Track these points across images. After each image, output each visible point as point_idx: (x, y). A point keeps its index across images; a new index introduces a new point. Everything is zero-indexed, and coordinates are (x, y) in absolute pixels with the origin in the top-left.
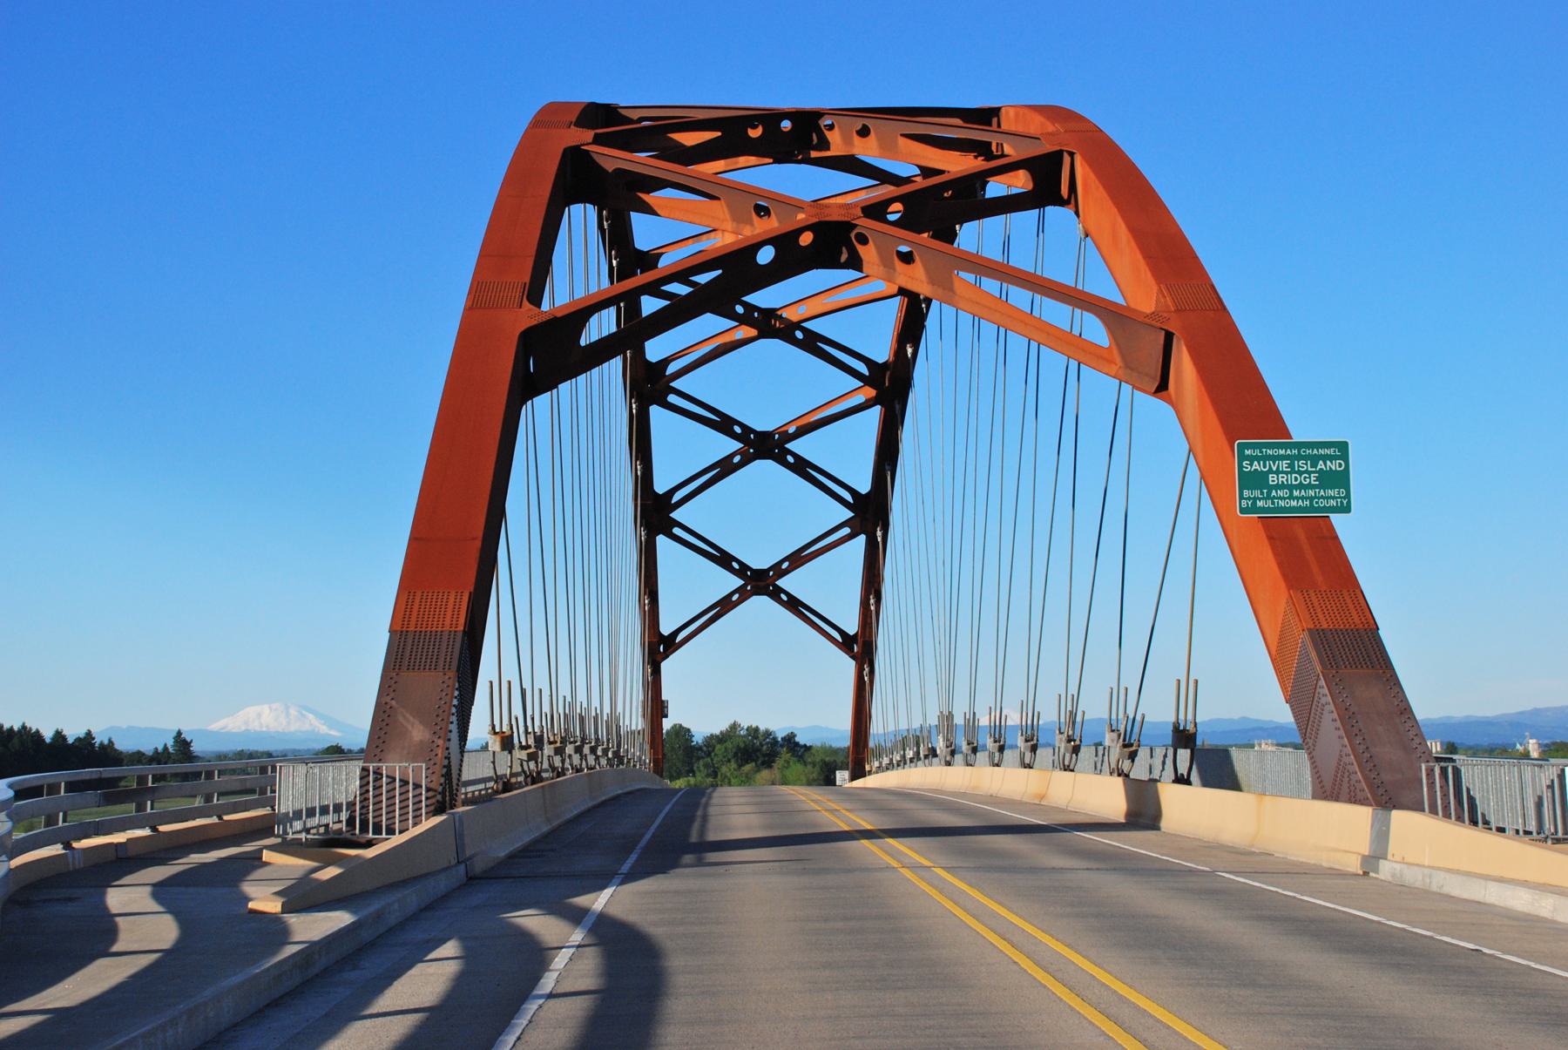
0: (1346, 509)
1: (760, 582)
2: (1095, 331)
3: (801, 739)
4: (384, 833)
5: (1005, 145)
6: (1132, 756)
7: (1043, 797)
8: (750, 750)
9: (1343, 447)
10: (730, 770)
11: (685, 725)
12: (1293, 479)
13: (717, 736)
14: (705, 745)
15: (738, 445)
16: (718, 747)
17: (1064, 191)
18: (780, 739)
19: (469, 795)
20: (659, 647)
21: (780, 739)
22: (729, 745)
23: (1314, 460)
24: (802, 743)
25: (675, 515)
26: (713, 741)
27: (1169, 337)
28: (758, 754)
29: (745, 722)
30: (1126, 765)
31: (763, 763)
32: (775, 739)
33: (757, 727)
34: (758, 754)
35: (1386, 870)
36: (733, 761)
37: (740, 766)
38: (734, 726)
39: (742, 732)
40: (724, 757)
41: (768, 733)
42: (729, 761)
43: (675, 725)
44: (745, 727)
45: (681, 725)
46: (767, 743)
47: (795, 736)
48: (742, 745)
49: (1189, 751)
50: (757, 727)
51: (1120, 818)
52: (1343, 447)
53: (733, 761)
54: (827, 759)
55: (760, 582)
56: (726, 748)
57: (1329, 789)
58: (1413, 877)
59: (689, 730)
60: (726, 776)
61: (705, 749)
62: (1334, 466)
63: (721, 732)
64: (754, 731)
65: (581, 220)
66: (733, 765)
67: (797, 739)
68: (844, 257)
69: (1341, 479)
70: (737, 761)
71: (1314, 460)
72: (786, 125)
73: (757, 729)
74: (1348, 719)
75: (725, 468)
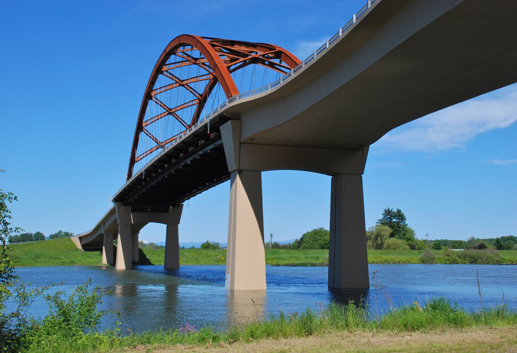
1: (170, 112)
11: (41, 232)
43: (37, 232)
45: (39, 232)
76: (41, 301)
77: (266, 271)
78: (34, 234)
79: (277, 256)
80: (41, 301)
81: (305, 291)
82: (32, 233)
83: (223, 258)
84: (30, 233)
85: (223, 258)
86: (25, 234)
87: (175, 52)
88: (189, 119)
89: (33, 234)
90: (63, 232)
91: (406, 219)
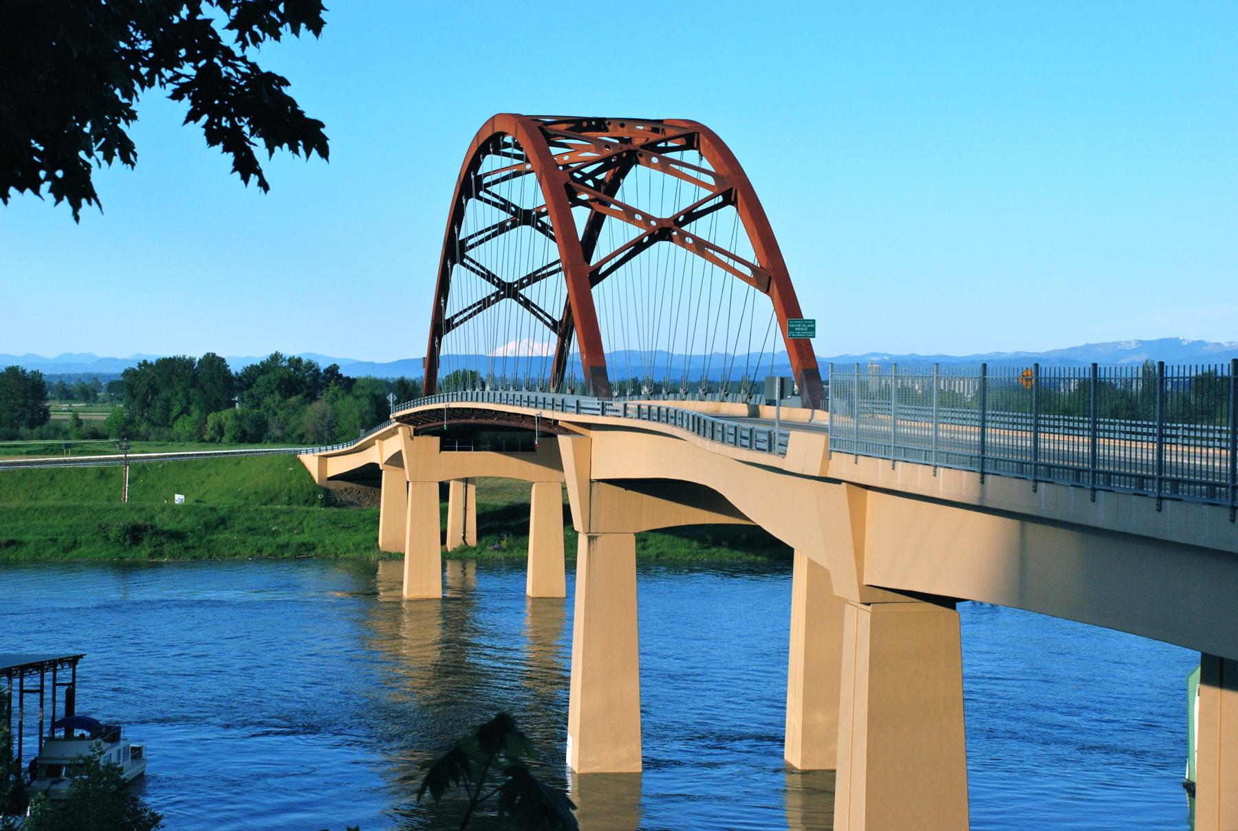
0: (814, 337)
1: (509, 290)
2: (747, 272)
3: (344, 372)
4: (449, 422)
5: (701, 135)
6: (751, 398)
7: (717, 411)
8: (294, 382)
9: (814, 321)
10: (275, 401)
11: (218, 354)
12: (802, 329)
13: (257, 367)
14: (245, 376)
15: (509, 216)
16: (260, 379)
17: (733, 199)
18: (322, 371)
19: (618, 405)
20: (441, 326)
21: (322, 371)
22: (272, 376)
23: (807, 324)
24: (345, 375)
25: (467, 253)
26: (254, 373)
27: (770, 278)
28: (303, 386)
29: (290, 350)
30: (748, 400)
31: (307, 395)
32: (317, 371)
33: (300, 358)
34: (303, 386)
35: (813, 421)
36: (276, 392)
37: (285, 398)
38: (276, 357)
39: (283, 363)
40: (267, 388)
41: (310, 365)
42: (272, 392)
43: (208, 354)
44: (287, 358)
45: (214, 355)
46: (310, 375)
47: (338, 368)
48: (286, 376)
49: (957, 604)
50: (300, 358)
51: (747, 415)
52: (814, 321)
53: (276, 392)
54: (376, 392)
55: (509, 290)
56: (269, 379)
57: (804, 406)
58: (817, 422)
59: (223, 360)
60: (270, 408)
61: (245, 380)
62: (812, 326)
63: (262, 363)
64: (296, 362)
65: (603, 248)
66: (278, 397)
67: (340, 372)
68: (667, 237)
69: (813, 329)
70: (280, 393)
71: (807, 324)
72: (624, 155)
73: (299, 361)
74: (810, 390)
75: (501, 228)
76: (382, 662)
77: (574, 602)
78: (197, 360)
79: (211, 426)
80: (382, 662)
81: (1202, 539)
82: (194, 356)
83: (207, 437)
84: (184, 357)
85: (207, 437)
86: (170, 358)
87: (59, 174)
88: (459, 279)
89: (195, 359)
90: (284, 357)
91: (296, 151)
